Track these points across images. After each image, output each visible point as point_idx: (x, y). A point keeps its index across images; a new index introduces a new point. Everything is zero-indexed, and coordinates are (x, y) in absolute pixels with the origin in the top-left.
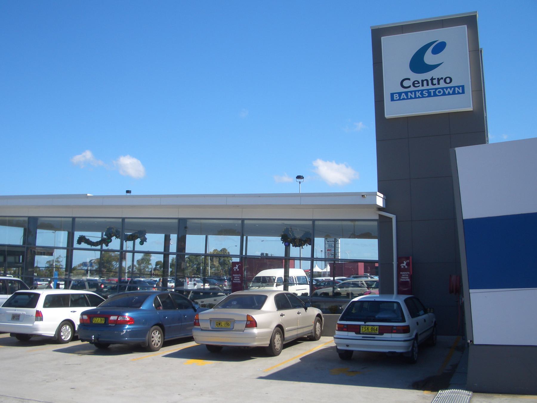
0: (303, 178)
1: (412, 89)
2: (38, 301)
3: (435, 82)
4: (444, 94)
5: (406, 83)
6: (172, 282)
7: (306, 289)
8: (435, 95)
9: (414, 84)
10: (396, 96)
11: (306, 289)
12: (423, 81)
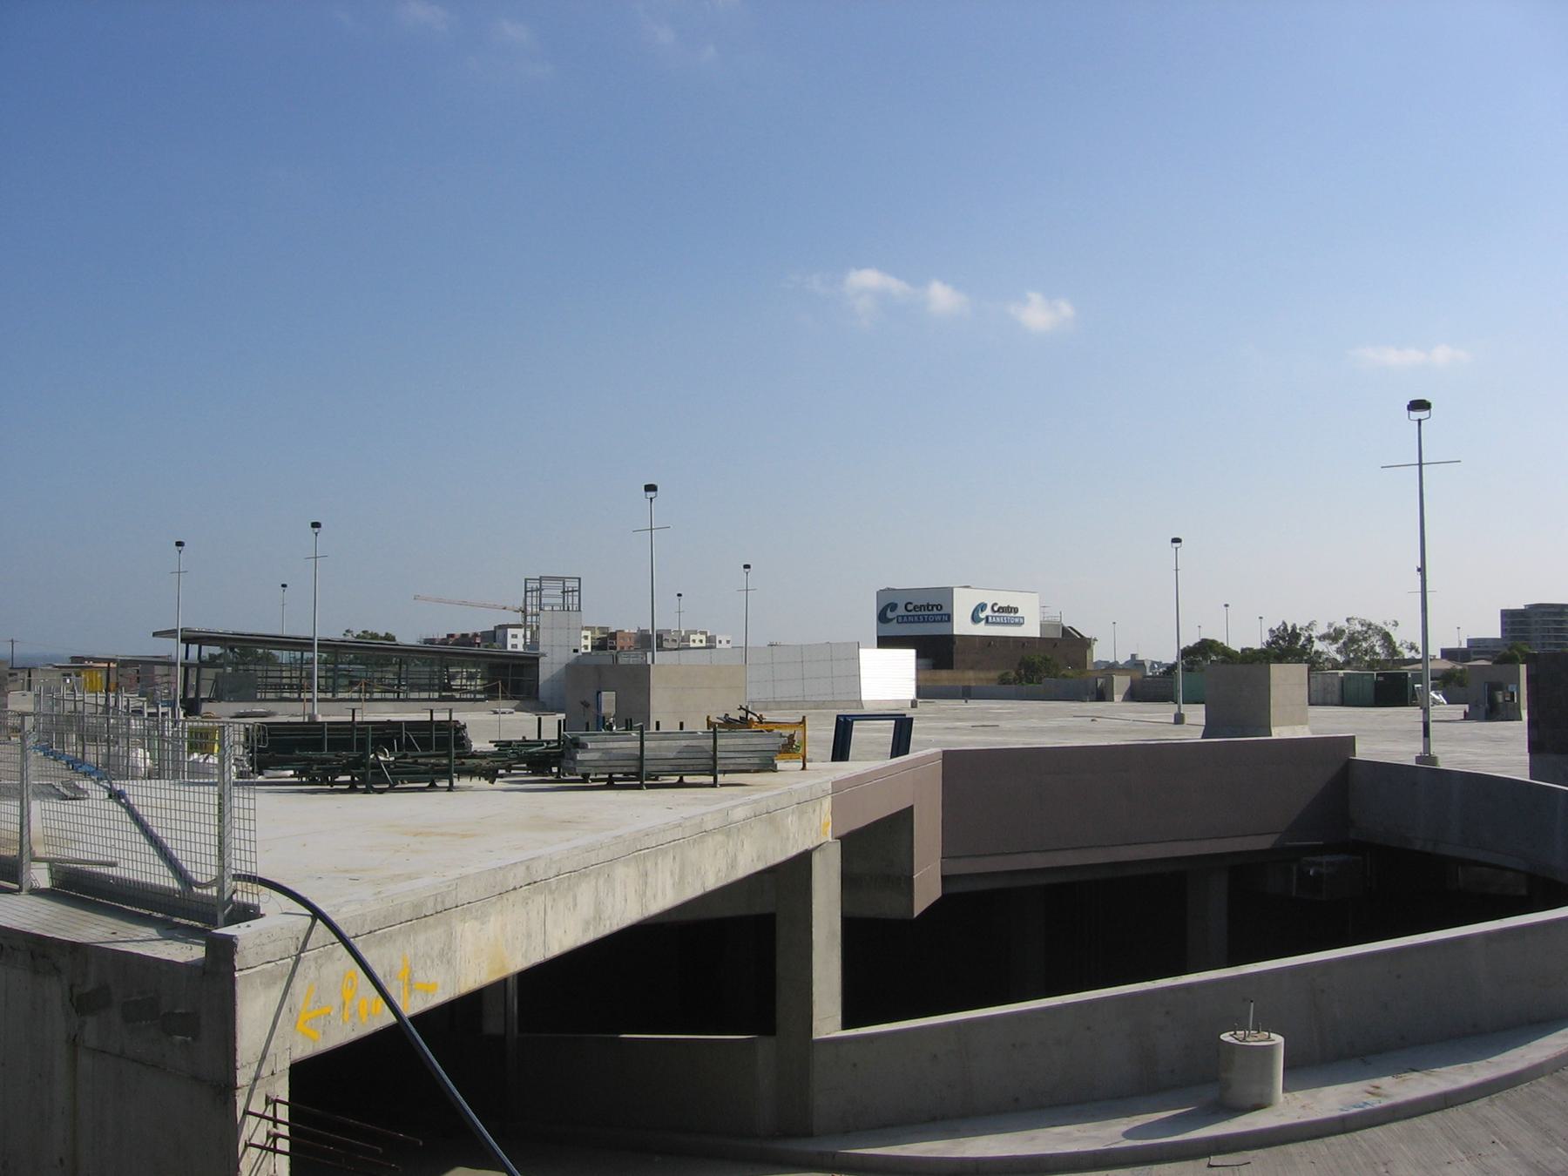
0: (1295, 625)
1: (913, 613)
2: (1391, 938)
3: (930, 608)
4: (934, 621)
5: (910, 607)
6: (1439, 687)
7: (1459, 461)
8: (928, 621)
9: (914, 608)
10: (515, 636)
11: (1459, 461)
12: (921, 606)
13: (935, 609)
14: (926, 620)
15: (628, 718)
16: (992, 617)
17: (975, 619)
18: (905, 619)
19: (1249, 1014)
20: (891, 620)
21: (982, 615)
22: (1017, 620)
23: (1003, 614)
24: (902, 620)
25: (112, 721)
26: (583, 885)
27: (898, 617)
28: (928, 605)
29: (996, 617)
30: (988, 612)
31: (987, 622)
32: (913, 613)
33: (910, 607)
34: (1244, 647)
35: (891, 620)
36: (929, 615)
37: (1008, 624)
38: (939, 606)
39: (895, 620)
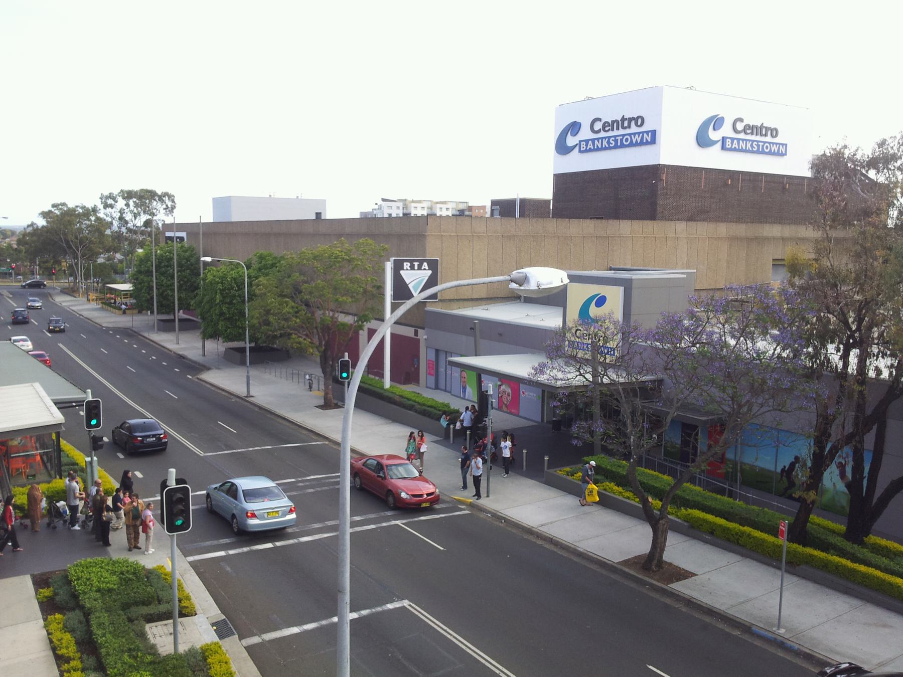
1: (603, 134)
3: (626, 124)
12: (613, 122)
13: (633, 123)
14: (619, 145)
15: (771, 263)
16: (732, 139)
17: (703, 140)
18: (590, 146)
19: (433, 545)
20: (714, 143)
21: (714, 135)
22: (775, 148)
23: (753, 138)
24: (588, 148)
25: (159, 252)
26: (452, 408)
27: (580, 142)
28: (623, 119)
29: (738, 140)
30: (726, 131)
31: (723, 148)
32: (603, 134)
33: (740, 126)
34: (34, 222)
35: (714, 143)
36: (623, 135)
37: (760, 151)
38: (639, 120)
39: (577, 149)
